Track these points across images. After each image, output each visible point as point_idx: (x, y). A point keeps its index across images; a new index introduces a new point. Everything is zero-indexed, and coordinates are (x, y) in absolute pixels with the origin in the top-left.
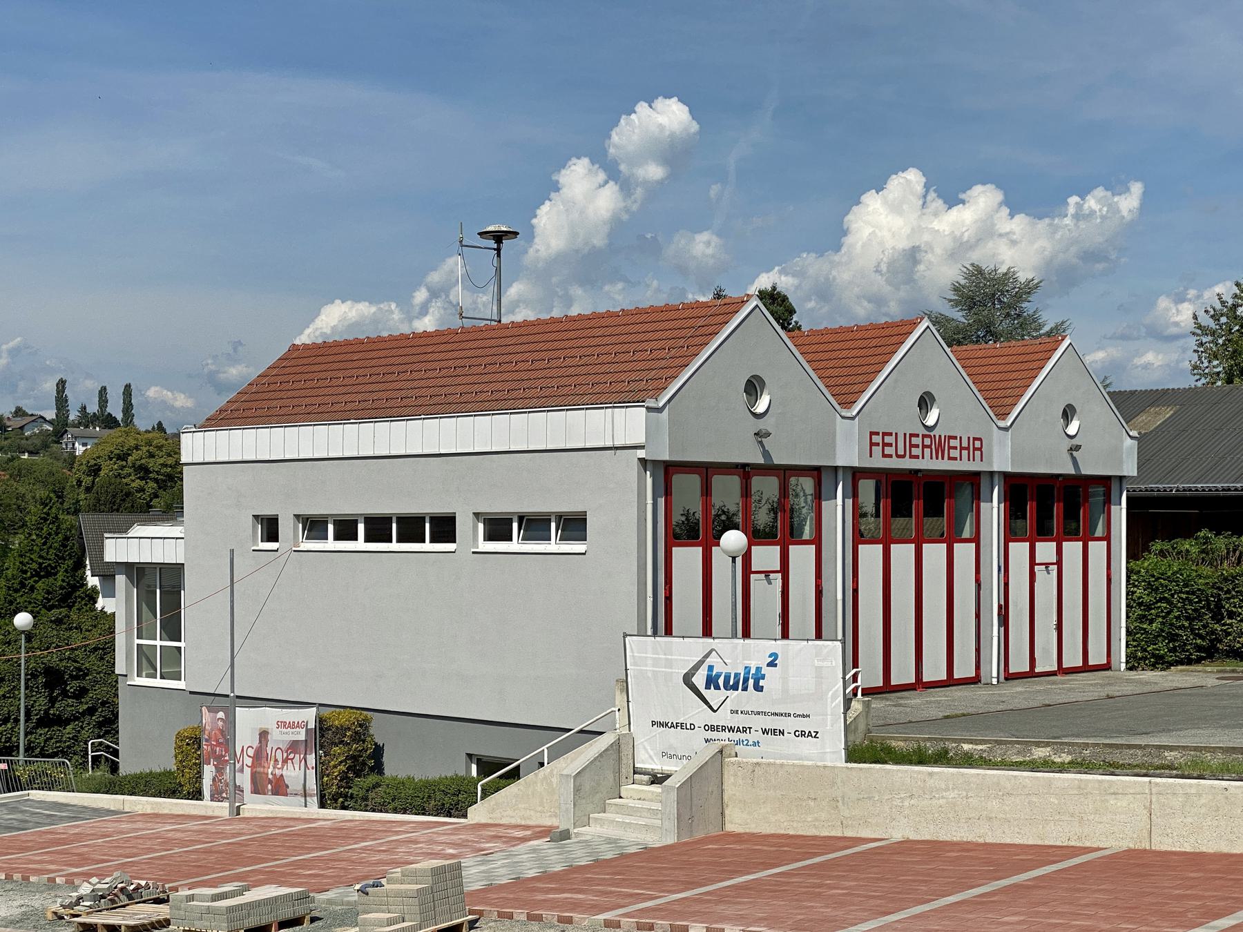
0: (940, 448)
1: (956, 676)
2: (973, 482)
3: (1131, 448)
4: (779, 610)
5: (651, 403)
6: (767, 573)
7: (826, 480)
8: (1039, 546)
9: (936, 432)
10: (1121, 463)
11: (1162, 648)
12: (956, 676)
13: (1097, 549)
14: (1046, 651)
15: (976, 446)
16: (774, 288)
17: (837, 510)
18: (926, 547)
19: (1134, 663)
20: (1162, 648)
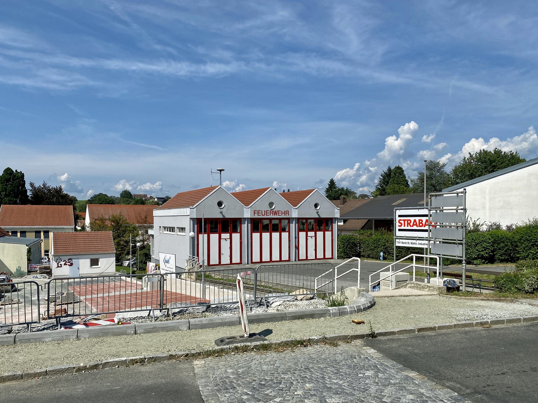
0: (275, 213)
1: (233, 262)
2: (289, 220)
3: (337, 212)
4: (229, 246)
5: (191, 207)
6: (225, 239)
7: (291, 220)
8: (212, 236)
9: (274, 210)
10: (334, 214)
11: (342, 255)
12: (233, 262)
13: (328, 234)
14: (311, 255)
15: (287, 212)
16: (44, 185)
17: (293, 226)
18: (263, 234)
19: (339, 257)
20: (342, 255)
